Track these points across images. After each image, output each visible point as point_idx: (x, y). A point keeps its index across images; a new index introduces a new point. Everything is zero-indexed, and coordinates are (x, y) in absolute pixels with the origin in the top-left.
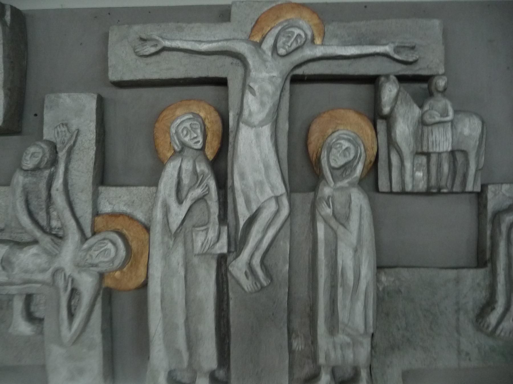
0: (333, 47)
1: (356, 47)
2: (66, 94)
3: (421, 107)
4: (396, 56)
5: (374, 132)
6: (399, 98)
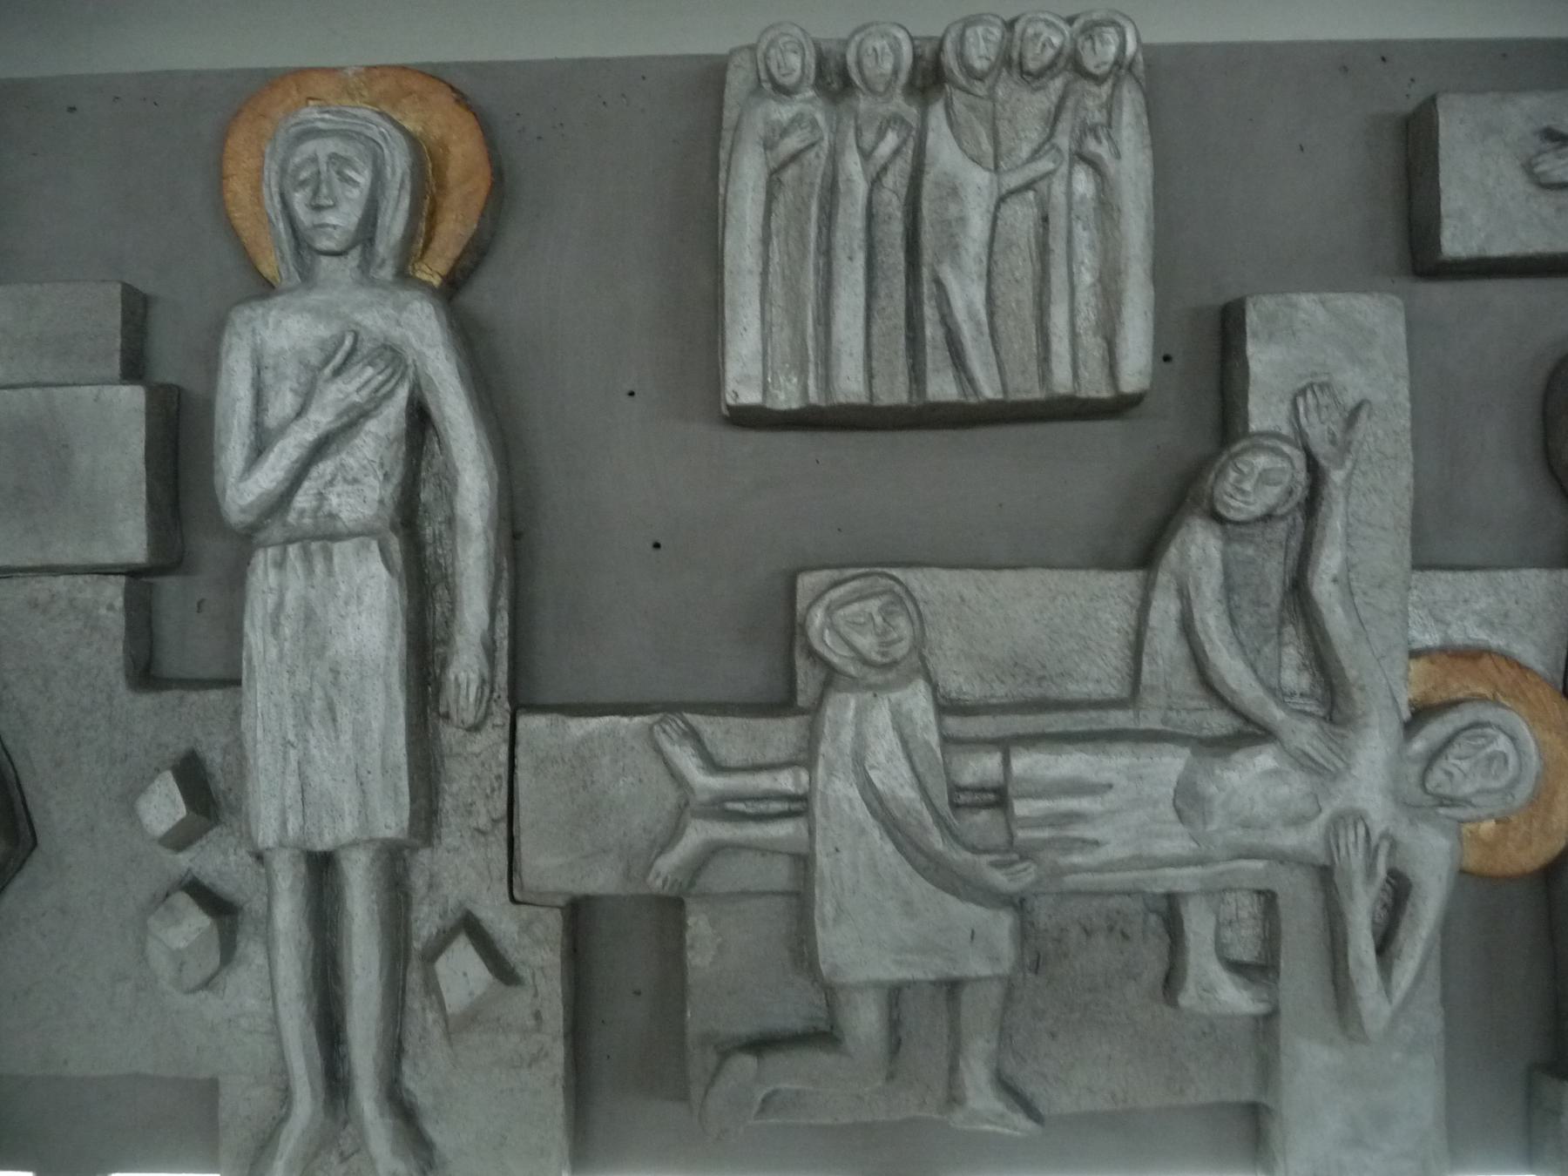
2: (1312, 296)
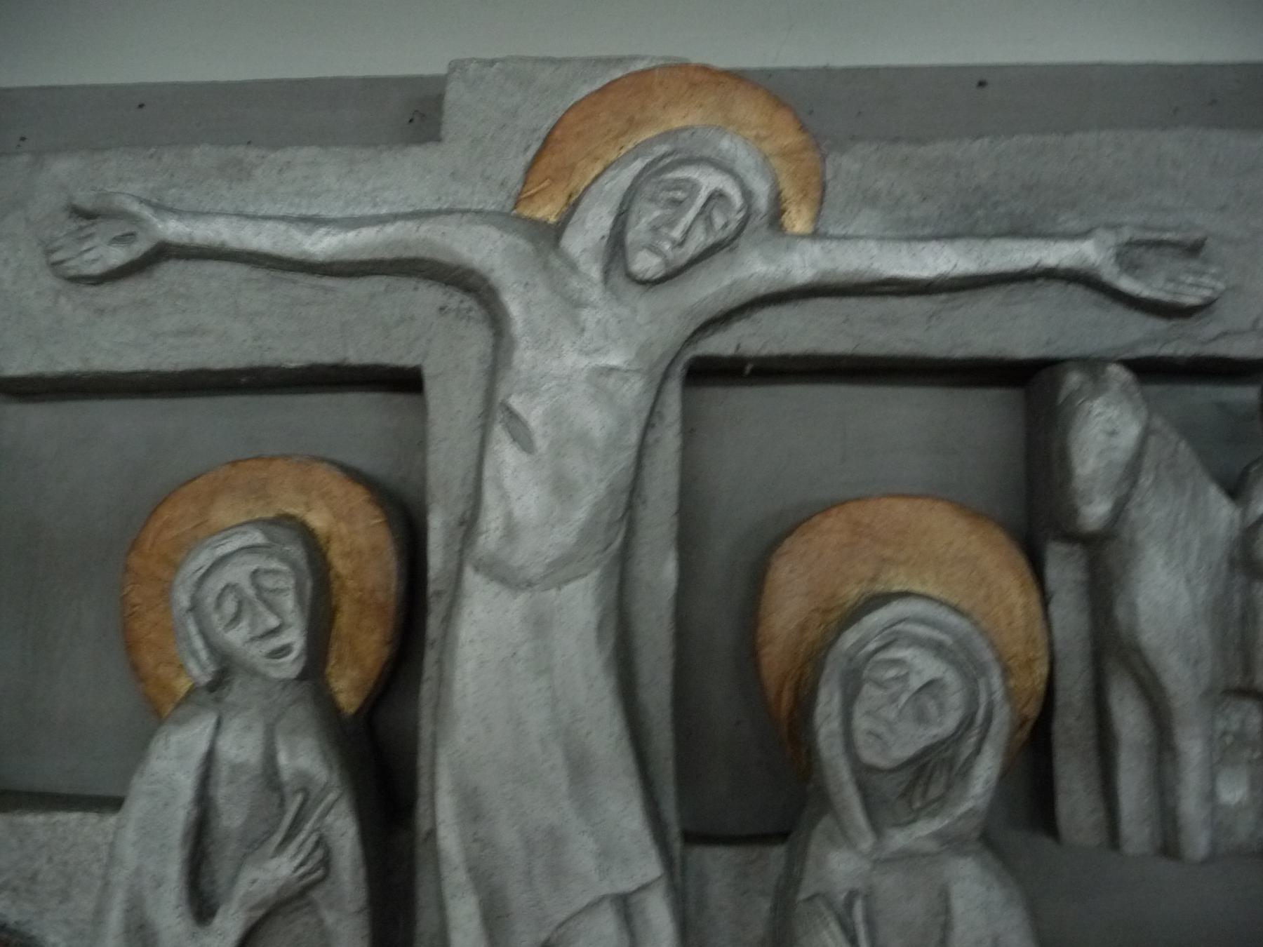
0: (861, 243)
1: (960, 244)
3: (1236, 490)
4: (1127, 284)
5: (1035, 597)
6: (1148, 462)
